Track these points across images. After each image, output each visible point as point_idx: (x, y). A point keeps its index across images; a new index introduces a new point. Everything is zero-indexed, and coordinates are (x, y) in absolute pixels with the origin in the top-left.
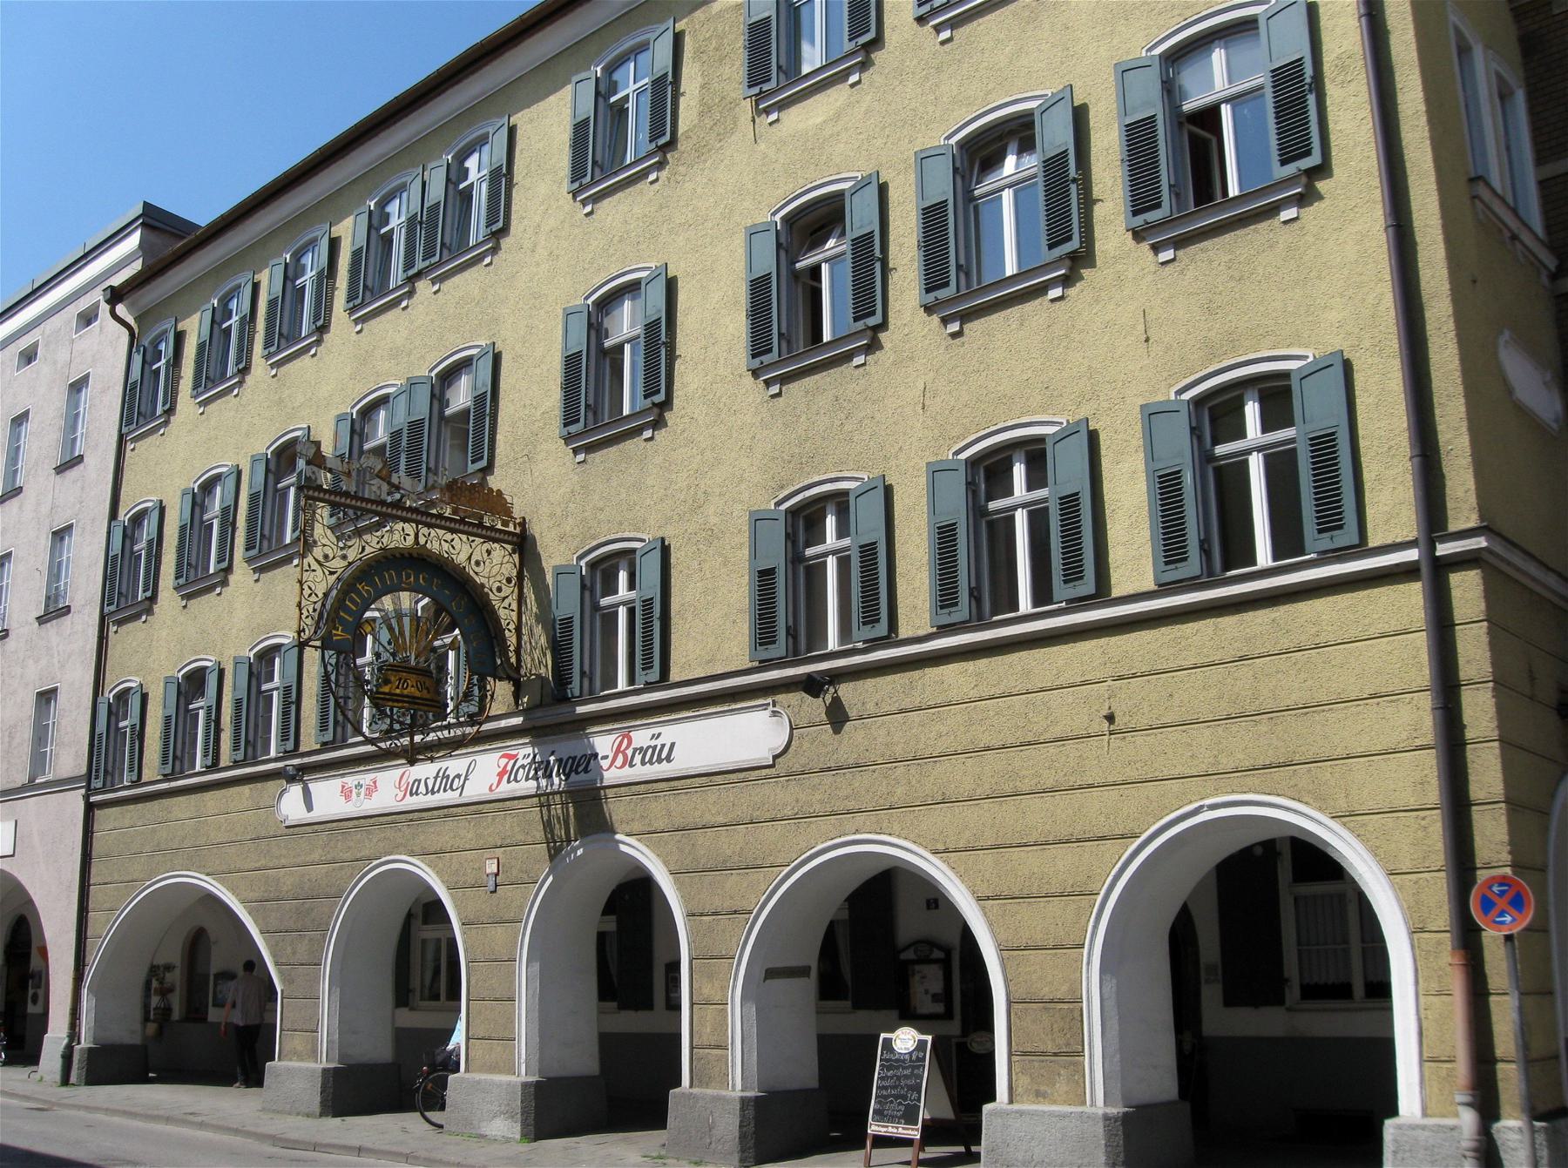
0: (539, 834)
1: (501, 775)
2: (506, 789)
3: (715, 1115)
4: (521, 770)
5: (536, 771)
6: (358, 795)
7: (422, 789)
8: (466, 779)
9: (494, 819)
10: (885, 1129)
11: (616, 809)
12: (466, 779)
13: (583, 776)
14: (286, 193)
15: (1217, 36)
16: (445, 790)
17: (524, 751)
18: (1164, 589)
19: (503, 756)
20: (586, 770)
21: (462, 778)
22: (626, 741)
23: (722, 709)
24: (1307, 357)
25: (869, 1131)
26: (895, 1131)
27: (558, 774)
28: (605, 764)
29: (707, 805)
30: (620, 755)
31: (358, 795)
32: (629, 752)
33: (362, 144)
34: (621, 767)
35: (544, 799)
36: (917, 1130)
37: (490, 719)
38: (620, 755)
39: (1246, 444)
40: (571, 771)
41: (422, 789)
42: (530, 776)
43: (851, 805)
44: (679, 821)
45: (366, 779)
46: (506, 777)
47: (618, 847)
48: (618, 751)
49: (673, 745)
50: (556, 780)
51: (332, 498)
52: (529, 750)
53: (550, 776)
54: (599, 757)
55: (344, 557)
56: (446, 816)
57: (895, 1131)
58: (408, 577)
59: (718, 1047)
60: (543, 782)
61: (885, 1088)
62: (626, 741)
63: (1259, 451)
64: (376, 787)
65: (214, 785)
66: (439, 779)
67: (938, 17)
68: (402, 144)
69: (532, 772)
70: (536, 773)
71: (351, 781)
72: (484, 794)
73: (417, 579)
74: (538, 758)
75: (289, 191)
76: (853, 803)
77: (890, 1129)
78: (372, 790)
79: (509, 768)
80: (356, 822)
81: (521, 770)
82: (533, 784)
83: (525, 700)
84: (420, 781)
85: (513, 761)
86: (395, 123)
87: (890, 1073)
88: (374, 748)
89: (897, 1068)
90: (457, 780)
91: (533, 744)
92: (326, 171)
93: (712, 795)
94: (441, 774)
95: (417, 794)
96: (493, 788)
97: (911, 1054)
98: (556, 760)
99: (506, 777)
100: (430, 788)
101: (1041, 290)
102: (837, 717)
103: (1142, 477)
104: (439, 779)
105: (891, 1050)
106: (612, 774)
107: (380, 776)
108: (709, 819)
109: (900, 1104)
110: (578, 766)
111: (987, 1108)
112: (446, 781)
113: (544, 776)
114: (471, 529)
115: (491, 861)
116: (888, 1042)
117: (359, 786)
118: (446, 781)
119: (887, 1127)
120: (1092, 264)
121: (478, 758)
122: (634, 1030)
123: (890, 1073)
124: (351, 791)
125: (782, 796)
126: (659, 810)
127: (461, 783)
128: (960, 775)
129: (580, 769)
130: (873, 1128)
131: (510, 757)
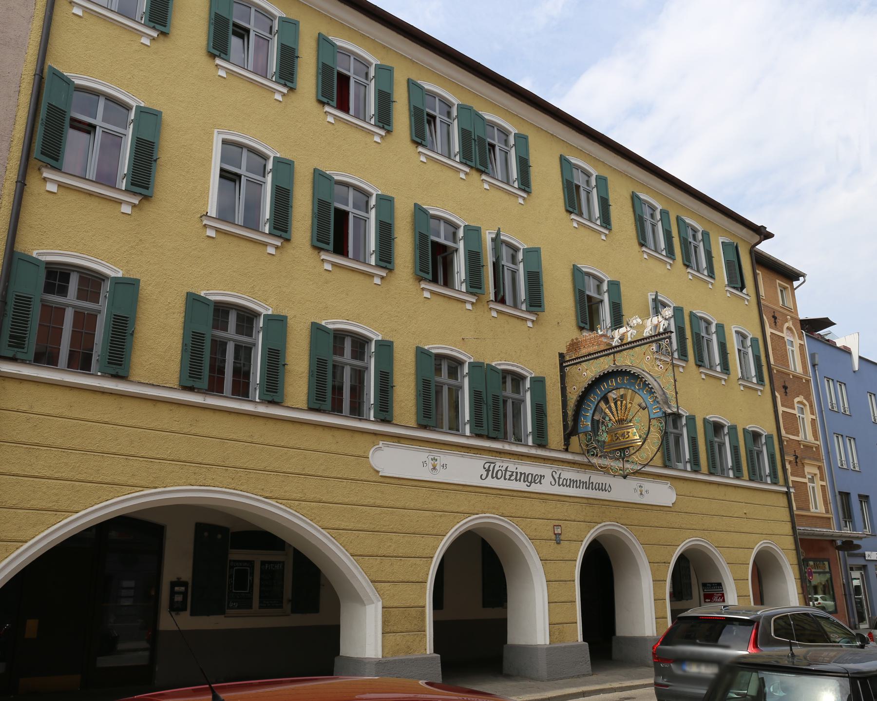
46: (490, 473)
58: (612, 382)
73: (616, 381)
79: (491, 468)
88: (586, 460)
111: (336, 659)
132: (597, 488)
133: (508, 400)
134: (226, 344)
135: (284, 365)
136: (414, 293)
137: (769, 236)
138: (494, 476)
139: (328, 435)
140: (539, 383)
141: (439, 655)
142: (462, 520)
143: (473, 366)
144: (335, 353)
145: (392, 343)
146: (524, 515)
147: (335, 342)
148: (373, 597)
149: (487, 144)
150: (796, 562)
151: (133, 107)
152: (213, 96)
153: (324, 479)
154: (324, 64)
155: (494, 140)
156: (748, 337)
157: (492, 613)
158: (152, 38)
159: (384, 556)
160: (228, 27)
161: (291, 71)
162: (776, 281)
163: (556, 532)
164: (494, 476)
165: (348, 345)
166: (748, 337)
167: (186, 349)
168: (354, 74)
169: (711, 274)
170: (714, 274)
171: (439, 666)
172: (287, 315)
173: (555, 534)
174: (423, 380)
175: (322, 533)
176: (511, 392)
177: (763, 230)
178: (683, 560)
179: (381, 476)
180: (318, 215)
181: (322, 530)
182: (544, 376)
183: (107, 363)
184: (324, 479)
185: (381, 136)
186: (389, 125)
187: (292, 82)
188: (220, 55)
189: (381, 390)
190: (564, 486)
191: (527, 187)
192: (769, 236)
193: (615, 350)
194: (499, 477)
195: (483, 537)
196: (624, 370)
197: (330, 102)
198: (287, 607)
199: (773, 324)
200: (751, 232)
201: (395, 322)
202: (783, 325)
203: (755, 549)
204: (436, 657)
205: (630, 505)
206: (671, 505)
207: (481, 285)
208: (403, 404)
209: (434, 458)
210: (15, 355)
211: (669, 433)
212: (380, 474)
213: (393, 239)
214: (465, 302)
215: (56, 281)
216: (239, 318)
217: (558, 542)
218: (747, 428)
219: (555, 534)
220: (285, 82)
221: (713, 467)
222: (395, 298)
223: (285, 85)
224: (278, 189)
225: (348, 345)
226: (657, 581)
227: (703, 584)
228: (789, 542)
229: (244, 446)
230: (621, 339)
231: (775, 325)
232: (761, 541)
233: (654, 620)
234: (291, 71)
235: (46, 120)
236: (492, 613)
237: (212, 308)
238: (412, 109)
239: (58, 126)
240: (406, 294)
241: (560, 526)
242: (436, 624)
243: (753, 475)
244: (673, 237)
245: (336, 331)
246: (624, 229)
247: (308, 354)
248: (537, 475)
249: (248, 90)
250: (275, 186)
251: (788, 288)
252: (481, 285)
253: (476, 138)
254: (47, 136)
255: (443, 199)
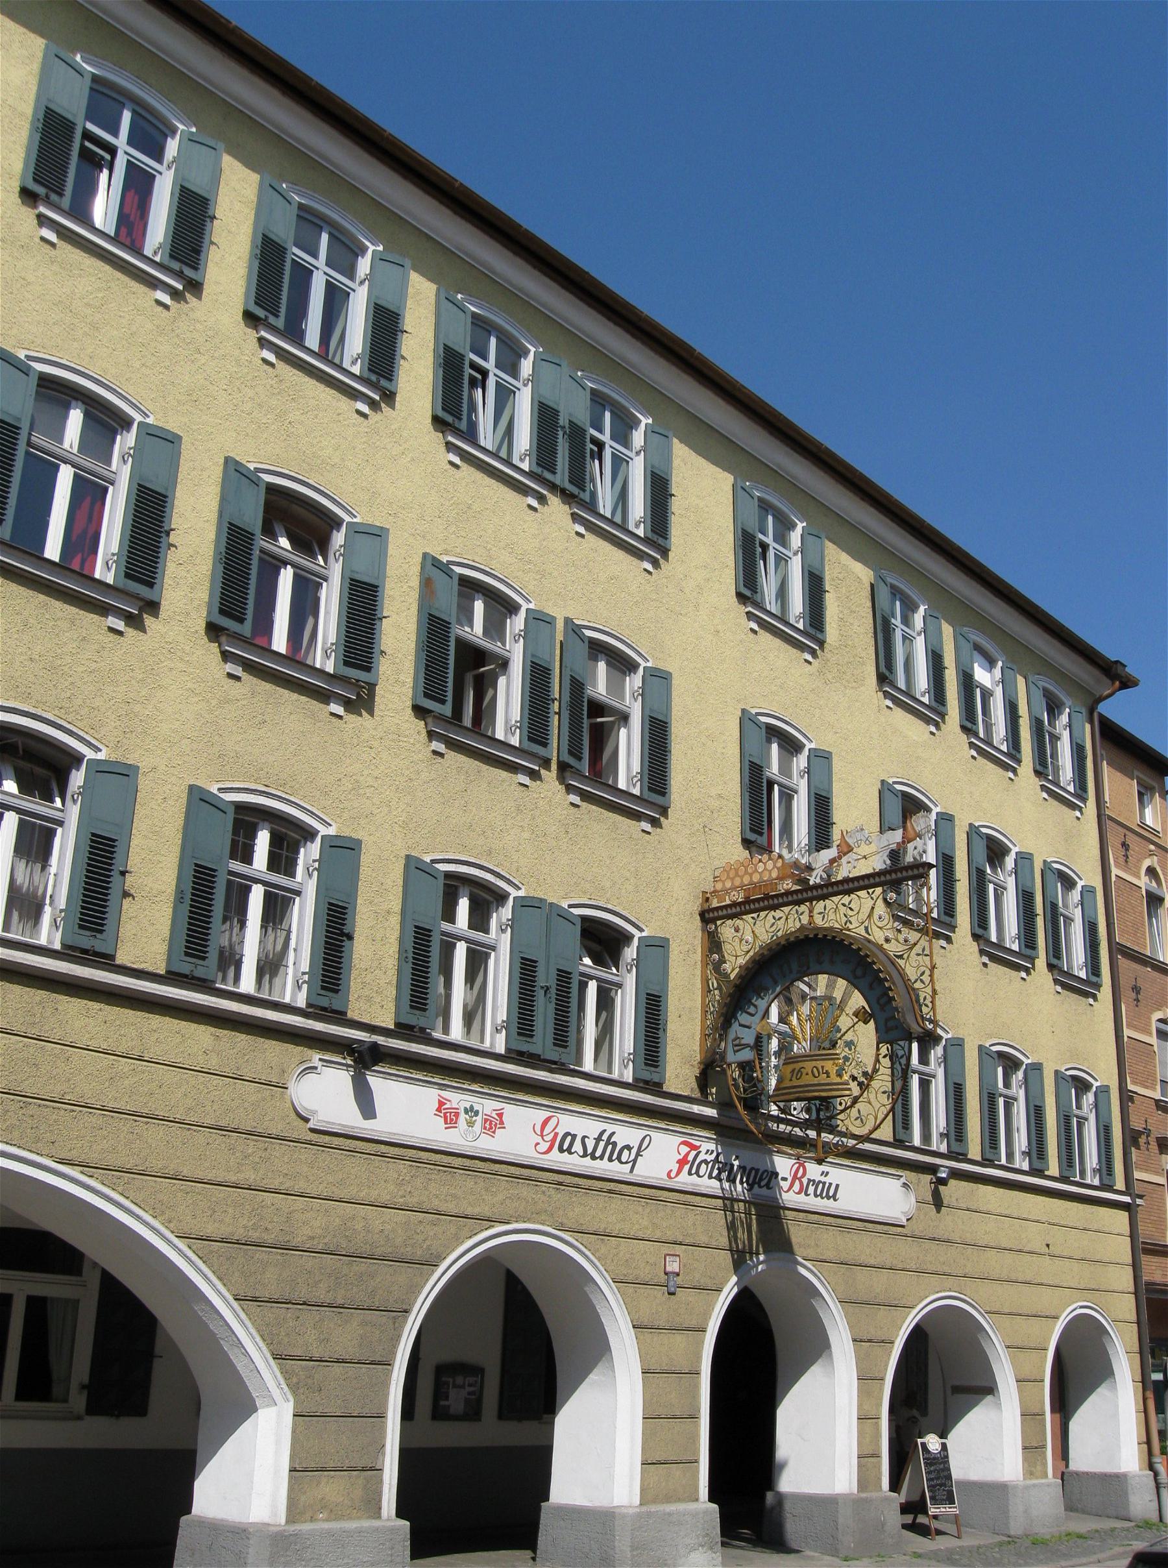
0: (724, 1241)
1: (682, 1162)
2: (685, 1180)
3: (885, 1513)
4: (703, 1166)
5: (720, 1171)
6: (471, 1124)
7: (577, 1147)
8: (638, 1154)
9: (822, 1232)
10: (938, 1510)
11: (797, 1233)
12: (638, 1154)
13: (764, 1191)
14: (590, 305)
15: (779, 735)
16: (610, 1160)
17: (708, 1147)
18: (172, 977)
19: (685, 1143)
20: (768, 1186)
21: (634, 1151)
22: (801, 1171)
23: (633, 1120)
24: (643, 931)
25: (930, 1513)
26: (944, 1510)
27: (742, 1183)
28: (785, 1185)
29: (863, 1246)
30: (797, 1181)
31: (471, 1124)
32: (805, 1181)
33: (298, 103)
34: (799, 1193)
35: (728, 1202)
36: (956, 1507)
37: (832, 1130)
38: (797, 1181)
39: (246, 870)
40: (754, 1182)
41: (577, 1147)
42: (714, 1175)
43: (947, 1270)
44: (844, 1257)
45: (488, 1106)
46: (687, 1167)
47: (797, 1269)
48: (795, 1177)
49: (837, 1186)
50: (739, 1188)
51: (888, 877)
52: (712, 1146)
53: (734, 1181)
54: (780, 1177)
55: (887, 940)
56: (610, 1192)
57: (944, 1510)
59: (872, 1456)
60: (726, 1185)
61: (932, 1480)
62: (801, 1171)
63: (466, 942)
64: (502, 1122)
65: (257, 1027)
66: (602, 1144)
67: (74, 223)
68: (520, 290)
69: (715, 1172)
70: (719, 1174)
71: (458, 1099)
72: (625, 1174)
74: (721, 1158)
75: (939, 554)
76: (947, 1268)
77: (948, 1510)
78: (494, 1124)
79: (690, 1158)
80: (467, 1162)
81: (703, 1166)
82: (715, 1183)
83: (714, 1090)
84: (574, 1137)
85: (695, 1152)
86: (545, 274)
87: (932, 1469)
89: (935, 1464)
90: (626, 1152)
91: (717, 1142)
92: (435, 203)
93: (866, 1238)
94: (605, 1137)
95: (570, 1153)
96: (673, 1175)
97: (940, 1453)
98: (739, 1167)
99: (687, 1167)
100: (590, 1151)
101: (513, 768)
102: (938, 1202)
103: (395, 921)
104: (602, 1144)
105: (928, 1452)
106: (790, 1197)
107: (510, 1110)
108: (863, 1259)
109: (944, 1490)
110: (761, 1179)
111: (184, 1519)
112: (610, 1148)
113: (728, 1180)
114: (757, 905)
115: (672, 1258)
116: (923, 1445)
117: (470, 1111)
118: (610, 1148)
119: (939, 1508)
120: (156, 615)
121: (655, 1135)
122: (34, 1445)
123: (932, 1469)
124: (457, 1115)
125: (905, 1251)
126: (830, 1242)
127: (632, 1157)
128: (995, 1263)
129: (763, 1183)
130: (933, 1510)
131: (693, 1147)
132: (824, 1195)
133: (590, 982)
134: (248, 889)
135: (123, 873)
136: (412, 741)
137: (1127, 683)
138: (694, 1171)
139: (203, 1034)
140: (657, 946)
141: (409, 1523)
142: (475, 1234)
143: (523, 904)
144: (233, 856)
145: (359, 842)
146: (605, 1228)
147: (235, 832)
148: (276, 1393)
149: (588, 440)
150: (1136, 1348)
151: (343, 523)
152: (24, 279)
153: (189, 1129)
154: (447, 348)
155: (485, 358)
156: (1011, 850)
157: (515, 1434)
158: (173, 291)
159: (304, 1304)
160: (70, 138)
161: (196, 244)
162: (1133, 772)
163: (669, 1269)
164: (694, 1171)
165: (263, 840)
166: (1011, 850)
167: (406, 957)
168: (327, 264)
169: (1079, 792)
170: (1020, 752)
171: (406, 1546)
172: (139, 764)
173: (666, 1274)
174: (196, 865)
175: (175, 1247)
176: (917, 1063)
177: (1120, 668)
178: (918, 1338)
179: (313, 1130)
180: (226, 558)
181: (176, 1241)
182: (668, 937)
183: (183, 953)
184: (189, 1129)
185: (370, 401)
186: (391, 380)
187: (196, 269)
188: (47, 196)
189: (326, 942)
190: (822, 1198)
191: (661, 536)
192: (1127, 683)
193: (815, 893)
194: (701, 1174)
195: (509, 1267)
196: (820, 936)
197: (272, 320)
198: (78, 1401)
199: (1122, 860)
200: (1096, 672)
201: (368, 798)
202: (1140, 861)
203: (1062, 1319)
204: (400, 1526)
205: (878, 1226)
206: (904, 1222)
207: (371, 663)
208: (370, 977)
209: (472, 1107)
210: (192, 971)
211: (996, 1096)
212: (311, 1125)
213: (381, 619)
214: (108, 610)
215: (283, 850)
216: (276, 841)
217: (673, 1289)
218: (1063, 1070)
219: (666, 1274)
220: (181, 267)
221: (991, 1147)
222: (371, 748)
223: (179, 275)
224: (433, 621)
225: (263, 840)
226: (867, 1379)
227: (952, 1387)
228: (1126, 1307)
229: (21, 1044)
230: (828, 871)
231: (1126, 862)
232: (1074, 1302)
233: (855, 1461)
234: (196, 244)
235: (227, 553)
236: (515, 1434)
237: (231, 815)
238: (441, 350)
239: (143, 519)
240: (393, 740)
241: (679, 1256)
242: (406, 1455)
243: (1068, 1166)
244: (825, 591)
245: (240, 807)
246: (850, 643)
247: (178, 854)
248: (567, 1134)
249: (100, 275)
250: (349, 580)
251: (1154, 788)
252: (371, 663)
253: (567, 426)
254: (137, 544)
255: (489, 546)
